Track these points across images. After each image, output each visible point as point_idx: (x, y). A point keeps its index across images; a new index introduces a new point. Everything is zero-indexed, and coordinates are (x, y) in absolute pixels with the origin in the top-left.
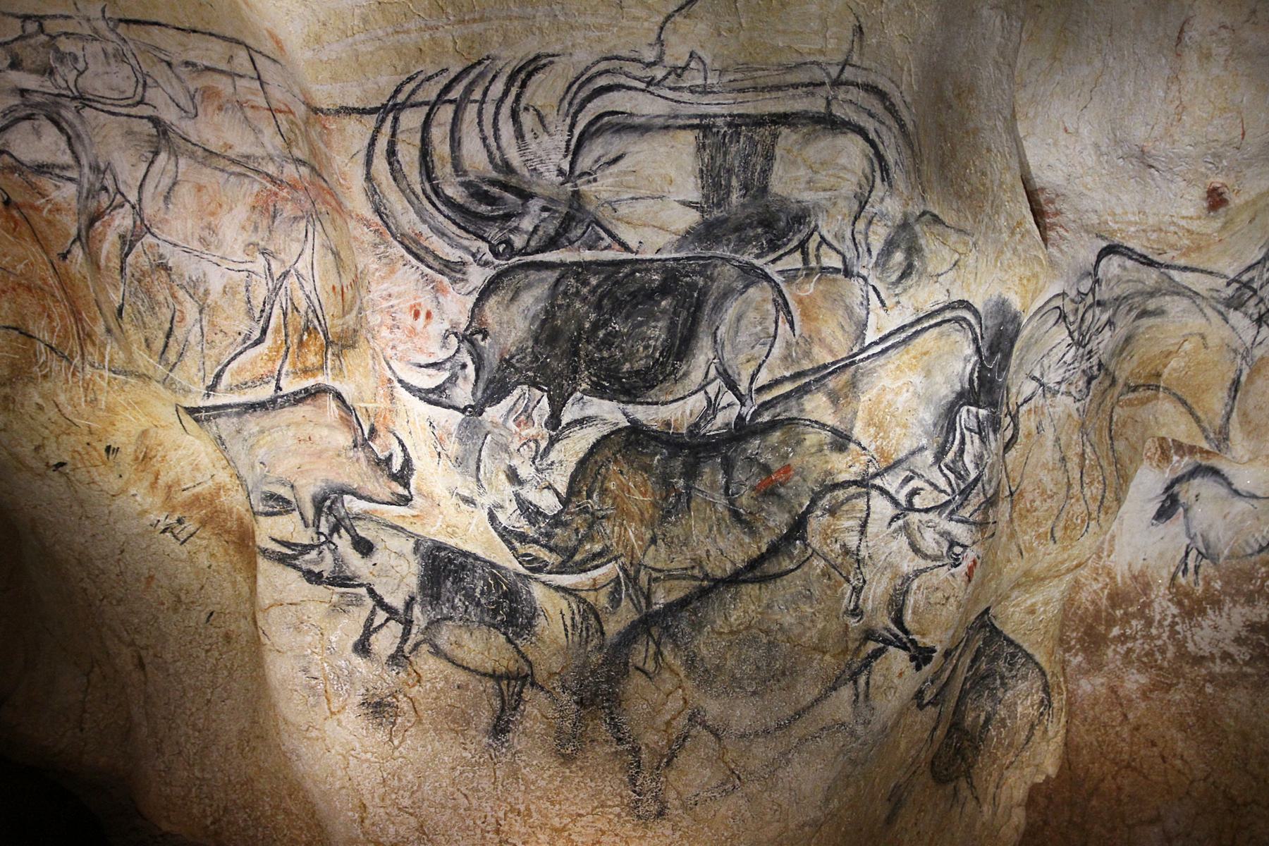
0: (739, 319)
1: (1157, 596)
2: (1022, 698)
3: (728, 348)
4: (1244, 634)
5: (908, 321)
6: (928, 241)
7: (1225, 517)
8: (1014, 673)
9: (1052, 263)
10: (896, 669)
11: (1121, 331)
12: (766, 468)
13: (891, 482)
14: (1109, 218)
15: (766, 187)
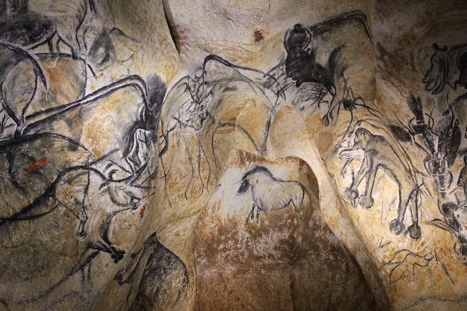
0: (15, 78)
1: (240, 229)
2: (175, 279)
3: (9, 94)
4: (278, 245)
5: (108, 83)
6: (117, 43)
7: (270, 191)
8: (170, 266)
9: (182, 61)
10: (104, 263)
11: (217, 97)
12: (32, 159)
13: (101, 167)
14: (210, 42)
15: (26, 7)
